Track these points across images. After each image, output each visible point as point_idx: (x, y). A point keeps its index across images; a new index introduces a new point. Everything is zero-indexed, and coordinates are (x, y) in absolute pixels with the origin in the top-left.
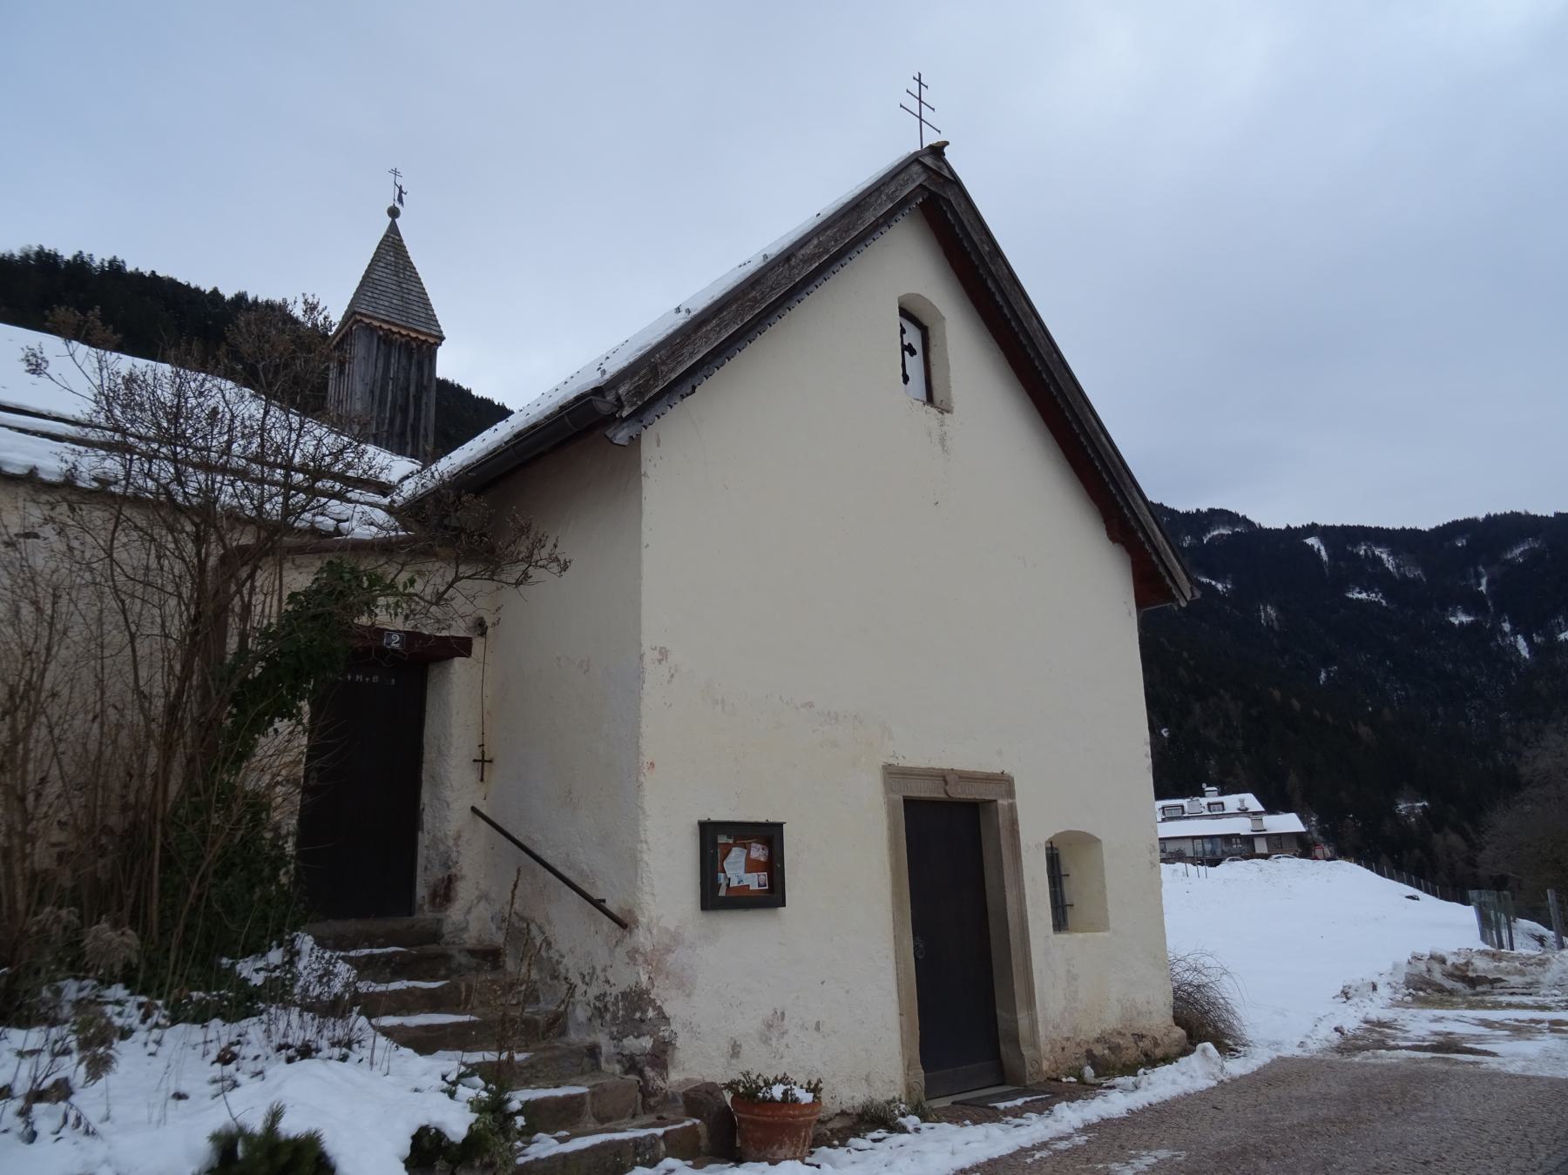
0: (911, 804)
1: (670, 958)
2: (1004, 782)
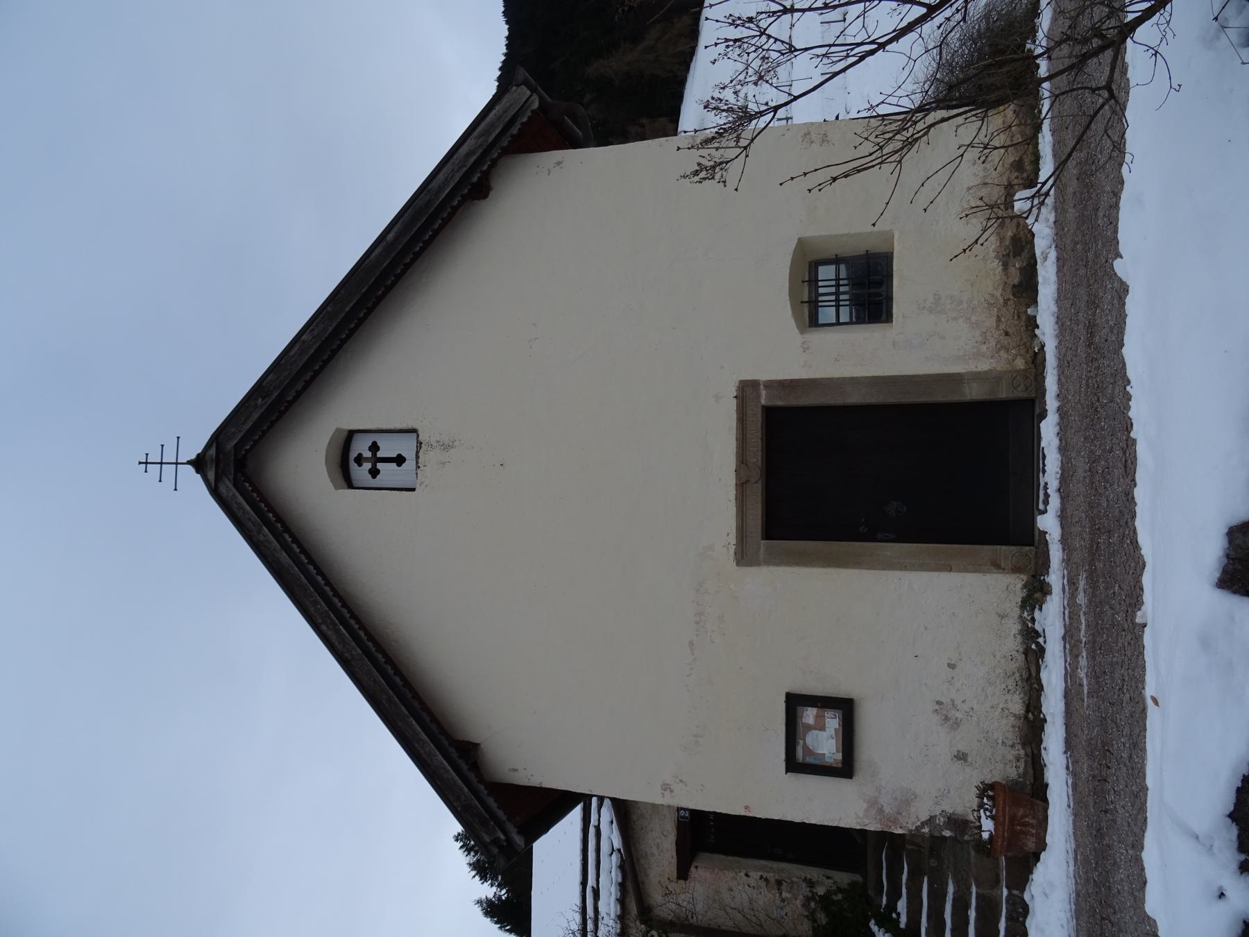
0: (770, 533)
1: (887, 810)
2: (746, 390)
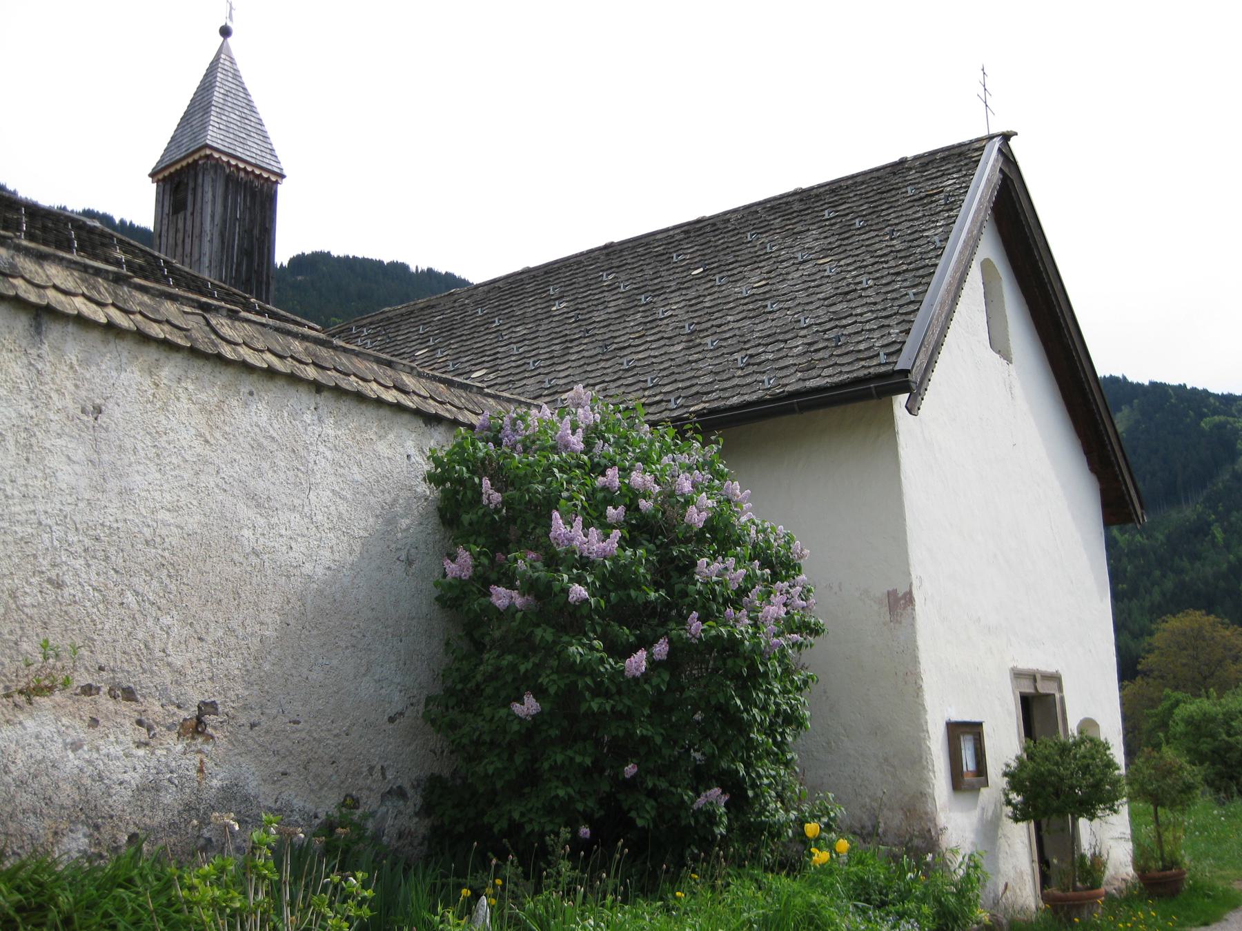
2: (1056, 678)
